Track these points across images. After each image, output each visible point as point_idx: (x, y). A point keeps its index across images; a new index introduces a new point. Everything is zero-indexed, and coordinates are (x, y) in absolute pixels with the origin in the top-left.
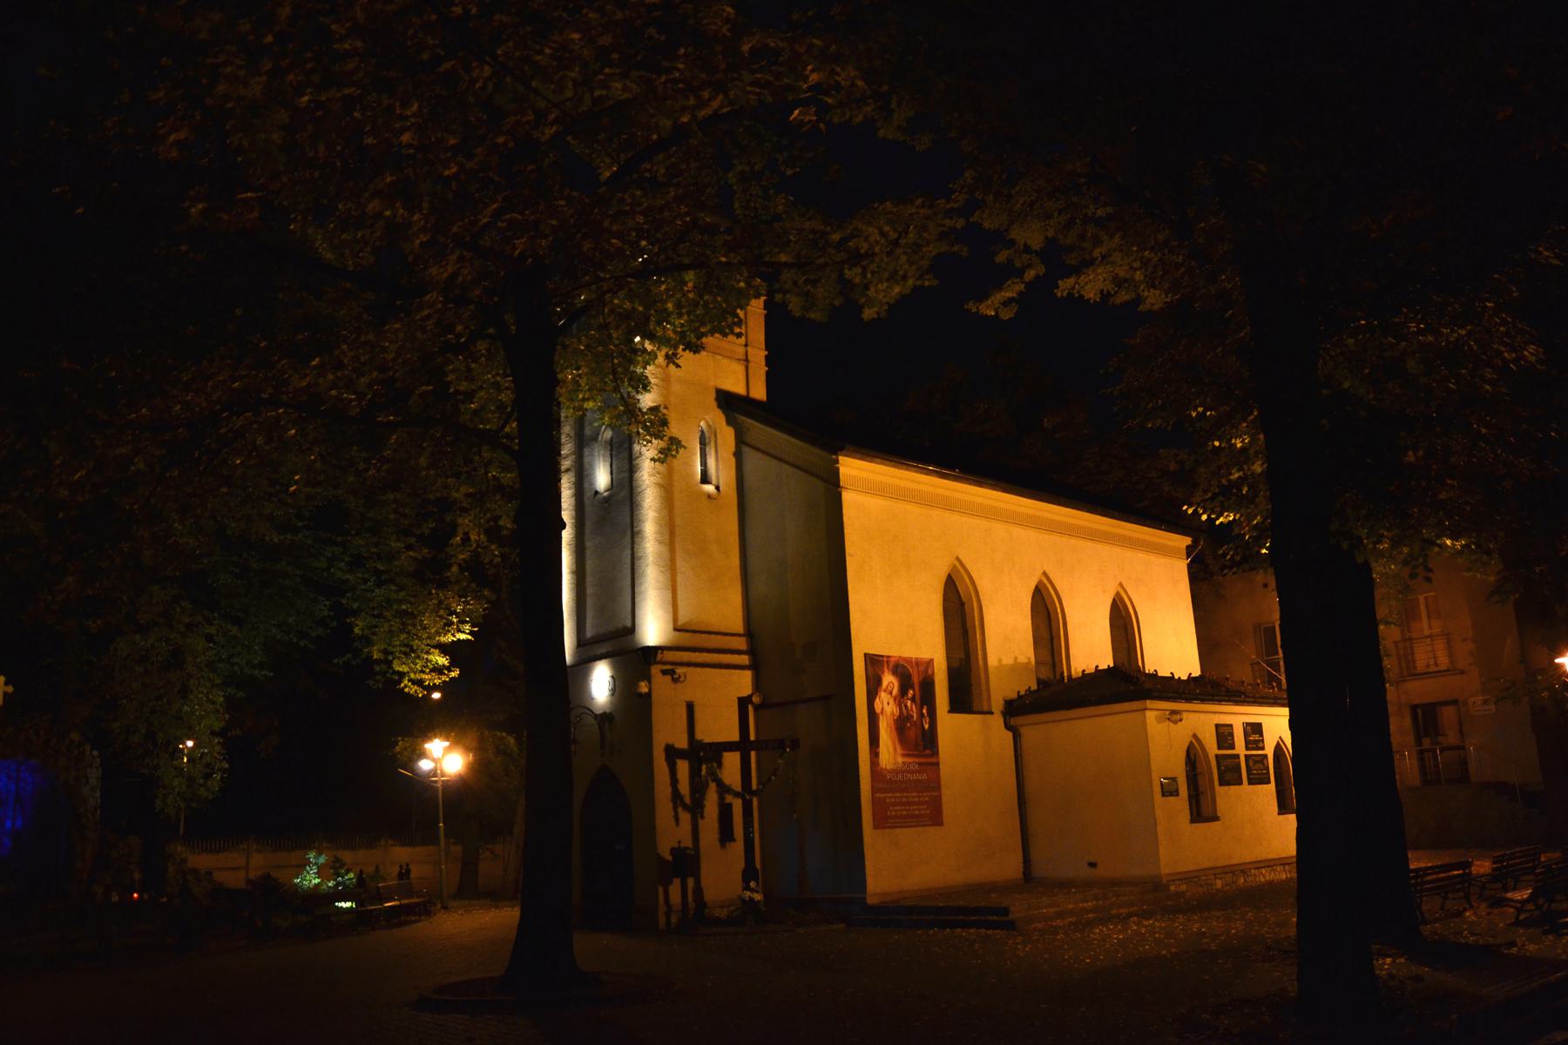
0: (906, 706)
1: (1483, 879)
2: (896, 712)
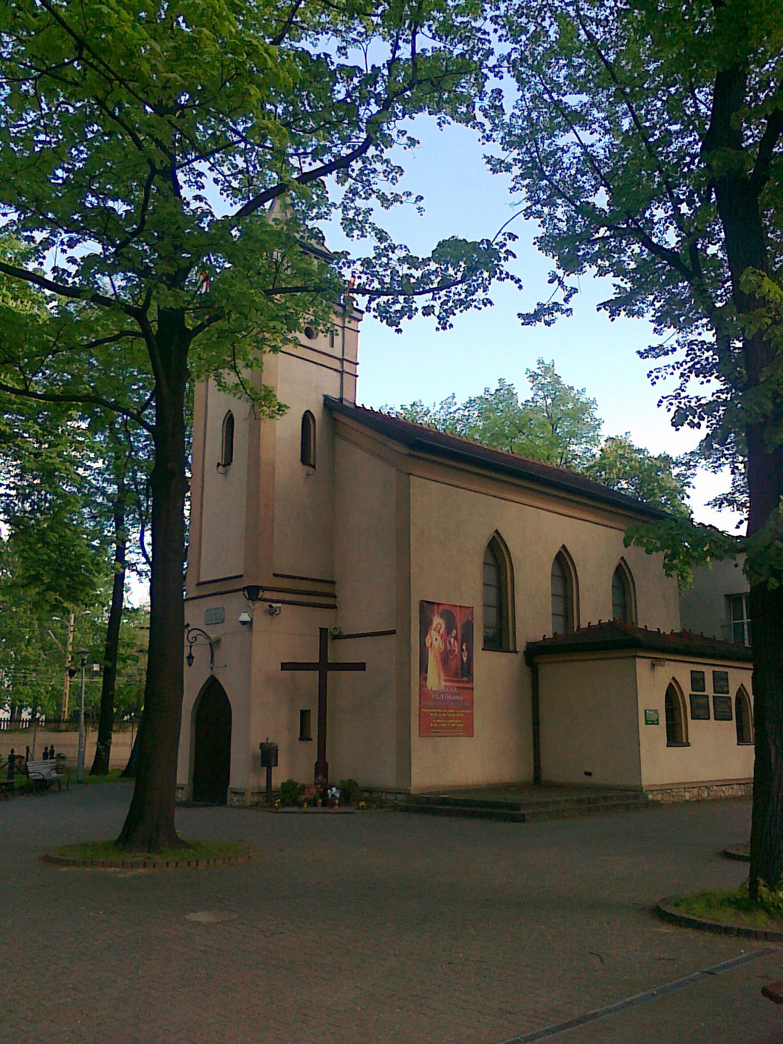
0: (450, 643)
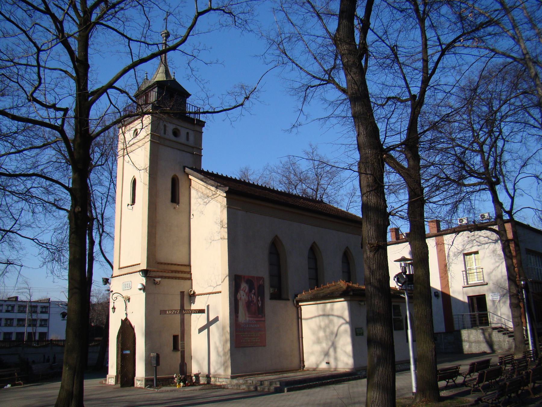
0: (251, 297)
1: (107, 15)
2: (247, 299)
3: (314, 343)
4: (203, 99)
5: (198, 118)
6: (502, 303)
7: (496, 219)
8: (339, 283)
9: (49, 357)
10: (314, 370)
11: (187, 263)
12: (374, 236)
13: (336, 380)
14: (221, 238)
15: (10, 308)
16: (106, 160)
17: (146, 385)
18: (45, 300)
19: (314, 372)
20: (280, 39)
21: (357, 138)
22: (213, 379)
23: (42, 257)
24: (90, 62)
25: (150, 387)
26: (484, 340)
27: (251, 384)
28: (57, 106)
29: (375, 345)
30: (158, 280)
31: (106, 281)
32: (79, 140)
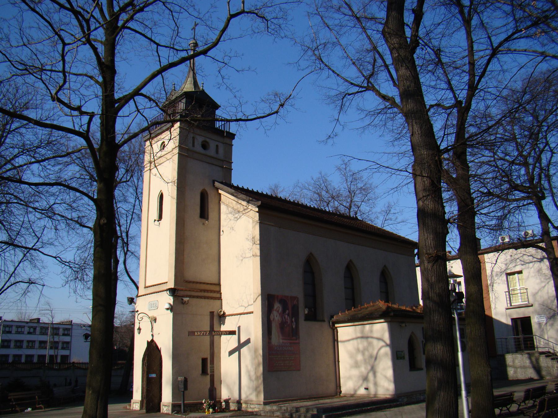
0: (285, 318)
3: (352, 367)
4: (236, 106)
5: (228, 131)
6: (549, 325)
7: (542, 235)
8: (377, 303)
9: (70, 380)
10: (352, 396)
11: (216, 282)
12: (432, 246)
13: (377, 407)
14: (253, 255)
15: (32, 330)
16: (132, 176)
17: (173, 411)
18: (67, 322)
19: (352, 398)
20: (315, 45)
21: (411, 138)
22: (244, 405)
23: (64, 276)
24: (117, 68)
25: (177, 413)
26: (531, 365)
27: (286, 411)
28: (83, 109)
29: (436, 367)
30: (186, 299)
31: (131, 301)
32: (105, 148)
